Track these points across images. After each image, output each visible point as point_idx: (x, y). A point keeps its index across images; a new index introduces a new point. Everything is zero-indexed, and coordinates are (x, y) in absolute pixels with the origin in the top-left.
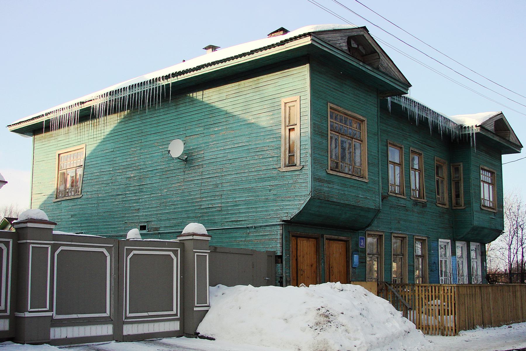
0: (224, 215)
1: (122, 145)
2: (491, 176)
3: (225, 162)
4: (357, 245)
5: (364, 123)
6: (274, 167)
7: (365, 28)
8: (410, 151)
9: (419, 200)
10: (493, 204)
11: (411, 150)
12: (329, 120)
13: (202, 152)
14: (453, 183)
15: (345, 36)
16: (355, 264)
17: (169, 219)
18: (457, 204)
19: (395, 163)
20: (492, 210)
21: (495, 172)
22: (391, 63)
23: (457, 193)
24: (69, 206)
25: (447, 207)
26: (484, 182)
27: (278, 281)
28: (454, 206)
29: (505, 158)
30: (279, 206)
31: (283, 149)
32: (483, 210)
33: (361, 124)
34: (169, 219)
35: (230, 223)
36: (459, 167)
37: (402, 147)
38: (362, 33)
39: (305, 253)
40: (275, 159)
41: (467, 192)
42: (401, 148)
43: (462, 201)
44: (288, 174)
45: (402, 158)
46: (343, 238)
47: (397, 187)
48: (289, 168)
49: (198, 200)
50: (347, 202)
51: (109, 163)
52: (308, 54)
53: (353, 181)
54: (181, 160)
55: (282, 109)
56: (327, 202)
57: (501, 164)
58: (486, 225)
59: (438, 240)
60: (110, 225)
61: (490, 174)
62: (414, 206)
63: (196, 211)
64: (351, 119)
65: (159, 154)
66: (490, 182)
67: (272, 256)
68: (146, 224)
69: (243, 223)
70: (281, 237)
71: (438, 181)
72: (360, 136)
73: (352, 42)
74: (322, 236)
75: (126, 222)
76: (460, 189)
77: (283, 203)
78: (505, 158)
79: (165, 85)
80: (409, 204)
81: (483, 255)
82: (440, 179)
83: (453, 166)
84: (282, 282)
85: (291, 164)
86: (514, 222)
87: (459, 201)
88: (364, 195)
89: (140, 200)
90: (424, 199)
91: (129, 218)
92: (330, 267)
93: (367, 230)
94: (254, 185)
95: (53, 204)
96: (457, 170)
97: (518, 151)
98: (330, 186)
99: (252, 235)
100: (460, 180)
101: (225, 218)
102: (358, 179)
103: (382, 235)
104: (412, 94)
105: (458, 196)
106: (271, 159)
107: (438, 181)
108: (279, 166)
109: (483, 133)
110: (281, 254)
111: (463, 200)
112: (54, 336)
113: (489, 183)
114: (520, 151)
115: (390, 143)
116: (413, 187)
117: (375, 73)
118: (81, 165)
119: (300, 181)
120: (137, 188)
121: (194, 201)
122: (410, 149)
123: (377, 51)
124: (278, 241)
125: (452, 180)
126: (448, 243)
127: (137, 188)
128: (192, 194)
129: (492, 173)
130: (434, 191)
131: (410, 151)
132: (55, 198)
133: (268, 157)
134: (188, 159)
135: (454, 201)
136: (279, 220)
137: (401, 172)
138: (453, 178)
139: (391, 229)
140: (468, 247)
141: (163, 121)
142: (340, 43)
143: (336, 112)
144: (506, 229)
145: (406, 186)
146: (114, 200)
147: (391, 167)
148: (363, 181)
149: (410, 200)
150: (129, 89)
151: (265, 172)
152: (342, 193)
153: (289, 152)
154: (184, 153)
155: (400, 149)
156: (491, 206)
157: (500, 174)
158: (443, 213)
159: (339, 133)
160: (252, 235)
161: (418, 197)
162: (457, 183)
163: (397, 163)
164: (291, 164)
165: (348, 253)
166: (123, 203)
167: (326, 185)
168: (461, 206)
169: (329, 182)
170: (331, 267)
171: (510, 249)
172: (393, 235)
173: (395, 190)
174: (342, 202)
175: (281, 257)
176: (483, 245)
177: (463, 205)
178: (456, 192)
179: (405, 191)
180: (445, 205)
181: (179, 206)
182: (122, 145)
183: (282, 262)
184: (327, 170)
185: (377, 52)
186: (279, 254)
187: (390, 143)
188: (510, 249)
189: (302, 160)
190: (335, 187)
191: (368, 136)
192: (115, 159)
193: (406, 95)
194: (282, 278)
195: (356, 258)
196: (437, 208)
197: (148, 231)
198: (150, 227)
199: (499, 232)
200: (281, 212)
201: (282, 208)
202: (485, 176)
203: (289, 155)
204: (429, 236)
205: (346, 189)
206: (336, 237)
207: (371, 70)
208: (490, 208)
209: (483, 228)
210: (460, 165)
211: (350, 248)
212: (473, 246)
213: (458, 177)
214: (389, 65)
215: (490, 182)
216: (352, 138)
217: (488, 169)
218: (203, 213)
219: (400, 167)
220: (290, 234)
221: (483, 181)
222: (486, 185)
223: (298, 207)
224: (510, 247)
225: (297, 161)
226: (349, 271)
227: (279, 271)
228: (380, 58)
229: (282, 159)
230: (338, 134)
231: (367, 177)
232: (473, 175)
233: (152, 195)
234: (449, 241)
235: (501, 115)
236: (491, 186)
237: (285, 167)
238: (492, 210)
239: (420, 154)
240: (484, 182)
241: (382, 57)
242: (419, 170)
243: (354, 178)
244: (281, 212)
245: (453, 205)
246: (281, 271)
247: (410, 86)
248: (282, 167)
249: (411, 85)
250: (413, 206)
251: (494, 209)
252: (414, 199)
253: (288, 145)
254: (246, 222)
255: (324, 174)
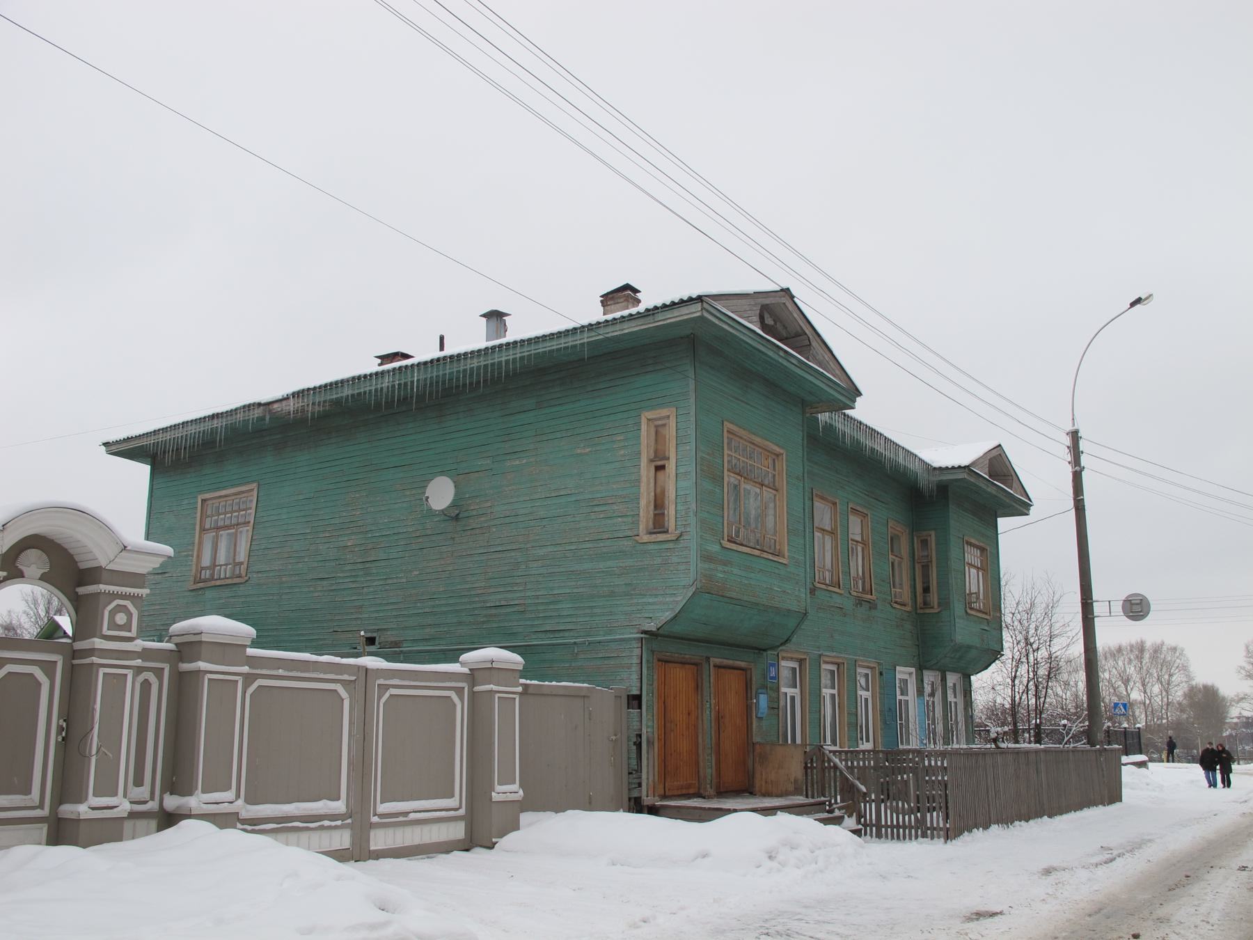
0: (529, 619)
1: (331, 487)
2: (981, 555)
3: (532, 523)
4: (764, 677)
5: (780, 457)
6: (626, 534)
7: (786, 291)
8: (849, 509)
9: (864, 596)
10: (984, 604)
11: (851, 508)
12: (726, 452)
13: (489, 504)
14: (917, 565)
15: (756, 305)
16: (761, 711)
17: (423, 627)
18: (926, 604)
19: (824, 530)
20: (984, 616)
21: (988, 549)
22: (830, 355)
23: (925, 585)
24: (220, 598)
25: (908, 608)
26: (971, 565)
27: (632, 743)
28: (921, 608)
29: (1003, 523)
30: (638, 604)
31: (643, 503)
32: (970, 615)
33: (776, 461)
34: (423, 627)
35: (543, 635)
36: (929, 539)
37: (836, 503)
38: (783, 300)
39: (678, 690)
40: (630, 519)
41: (944, 584)
42: (835, 504)
43: (934, 598)
44: (652, 547)
45: (836, 522)
46: (743, 664)
47: (827, 573)
48: (654, 536)
49: (480, 592)
50: (753, 599)
51: (304, 520)
52: (692, 334)
53: (763, 561)
54: (449, 516)
55: (643, 430)
56: (721, 598)
57: (997, 534)
58: (976, 642)
59: (895, 667)
60: (302, 635)
61: (978, 551)
62: (857, 606)
63: (476, 612)
64: (761, 450)
65: (405, 505)
66: (979, 566)
67: (621, 697)
68: (374, 635)
69: (567, 634)
70: (639, 662)
71: (893, 564)
72: (774, 482)
73: (766, 316)
74: (708, 659)
75: (335, 630)
76: (931, 578)
77: (644, 600)
78: (1003, 523)
79: (475, 368)
80: (848, 604)
81: (967, 691)
82: (897, 559)
83: (917, 537)
84: (640, 743)
85: (659, 524)
86: (1020, 637)
87: (928, 599)
88: (780, 587)
89: (365, 589)
90: (871, 595)
91: (341, 624)
92: (720, 717)
93: (781, 650)
94: (587, 566)
95: (189, 593)
96: (925, 543)
97: (1026, 511)
98: (726, 569)
99: (583, 656)
100: (931, 562)
101: (532, 626)
102: (771, 558)
103: (806, 659)
104: (861, 411)
105: (926, 590)
106: (620, 519)
107: (893, 564)
108: (636, 533)
109: (972, 480)
110: (638, 693)
111: (936, 595)
112: (134, 824)
113: (978, 568)
114: (1027, 512)
115: (817, 495)
116: (853, 573)
117: (803, 370)
118: (247, 520)
119: (675, 559)
120: (360, 566)
121: (473, 593)
122: (850, 507)
123: (807, 332)
124: (633, 669)
125: (916, 562)
126: (910, 674)
127: (360, 566)
128: (468, 579)
129: (983, 550)
130: (888, 581)
131: (849, 509)
132: (192, 583)
133: (615, 515)
134: (461, 516)
135: (920, 600)
136: (635, 631)
137: (835, 548)
138: (919, 559)
139: (819, 648)
140: (944, 679)
141: (507, 439)
142: (747, 315)
143: (736, 438)
144: (1007, 653)
145: (842, 572)
146: (312, 589)
147: (818, 537)
148: (780, 561)
149: (849, 595)
150: (293, 397)
151: (608, 543)
152: (746, 582)
153: (656, 507)
154: (454, 505)
155: (832, 505)
156: (982, 607)
157: (995, 552)
158: (903, 620)
159: (741, 476)
160: (583, 656)
161: (861, 590)
162: (926, 568)
163: (827, 531)
164: (659, 524)
165: (749, 691)
166: (332, 594)
167: (720, 568)
168: (933, 608)
169: (725, 563)
170: (722, 717)
171: (1013, 686)
172: (823, 658)
173: (825, 579)
174: (745, 598)
175: (638, 698)
176: (967, 678)
177: (936, 606)
178: (923, 583)
179: (841, 579)
180: (904, 605)
181: (443, 602)
182: (331, 487)
183: (640, 707)
184: (722, 541)
185: (806, 334)
186: (635, 692)
187: (817, 495)
188: (1013, 686)
189: (679, 523)
190: (736, 571)
191: (787, 482)
192: (316, 513)
193: (848, 412)
194: (640, 736)
195: (763, 700)
196: (893, 611)
197: (379, 647)
198: (382, 639)
199: (994, 654)
200: (639, 616)
201: (639, 607)
202: (973, 556)
203: (656, 512)
204: (881, 662)
205: (752, 575)
206: (730, 662)
207: (796, 366)
208: (980, 611)
209: (969, 647)
210: (930, 535)
211: (754, 682)
212: (952, 679)
213: (928, 556)
214: (826, 357)
215: (979, 566)
216: (762, 485)
217: (977, 543)
218: (491, 615)
219: (832, 537)
220: (655, 657)
221: (969, 564)
222: (973, 571)
223: (671, 606)
224: (1013, 681)
225: (671, 524)
226: (752, 723)
227: (635, 723)
228: (810, 344)
229: (641, 519)
230: (739, 478)
231: (786, 554)
232: (954, 553)
233: (389, 582)
234: (913, 670)
235: (1000, 448)
236: (980, 574)
237: (647, 534)
238: (984, 616)
239: (865, 515)
240: (971, 565)
241: (814, 344)
242: (864, 542)
243: (765, 555)
244: (639, 616)
245: (918, 607)
246: (638, 724)
247: (859, 394)
248: (641, 534)
249: (860, 392)
250: (854, 607)
251: (986, 613)
252: (855, 594)
253: (653, 494)
254: (572, 634)
255: (716, 548)
